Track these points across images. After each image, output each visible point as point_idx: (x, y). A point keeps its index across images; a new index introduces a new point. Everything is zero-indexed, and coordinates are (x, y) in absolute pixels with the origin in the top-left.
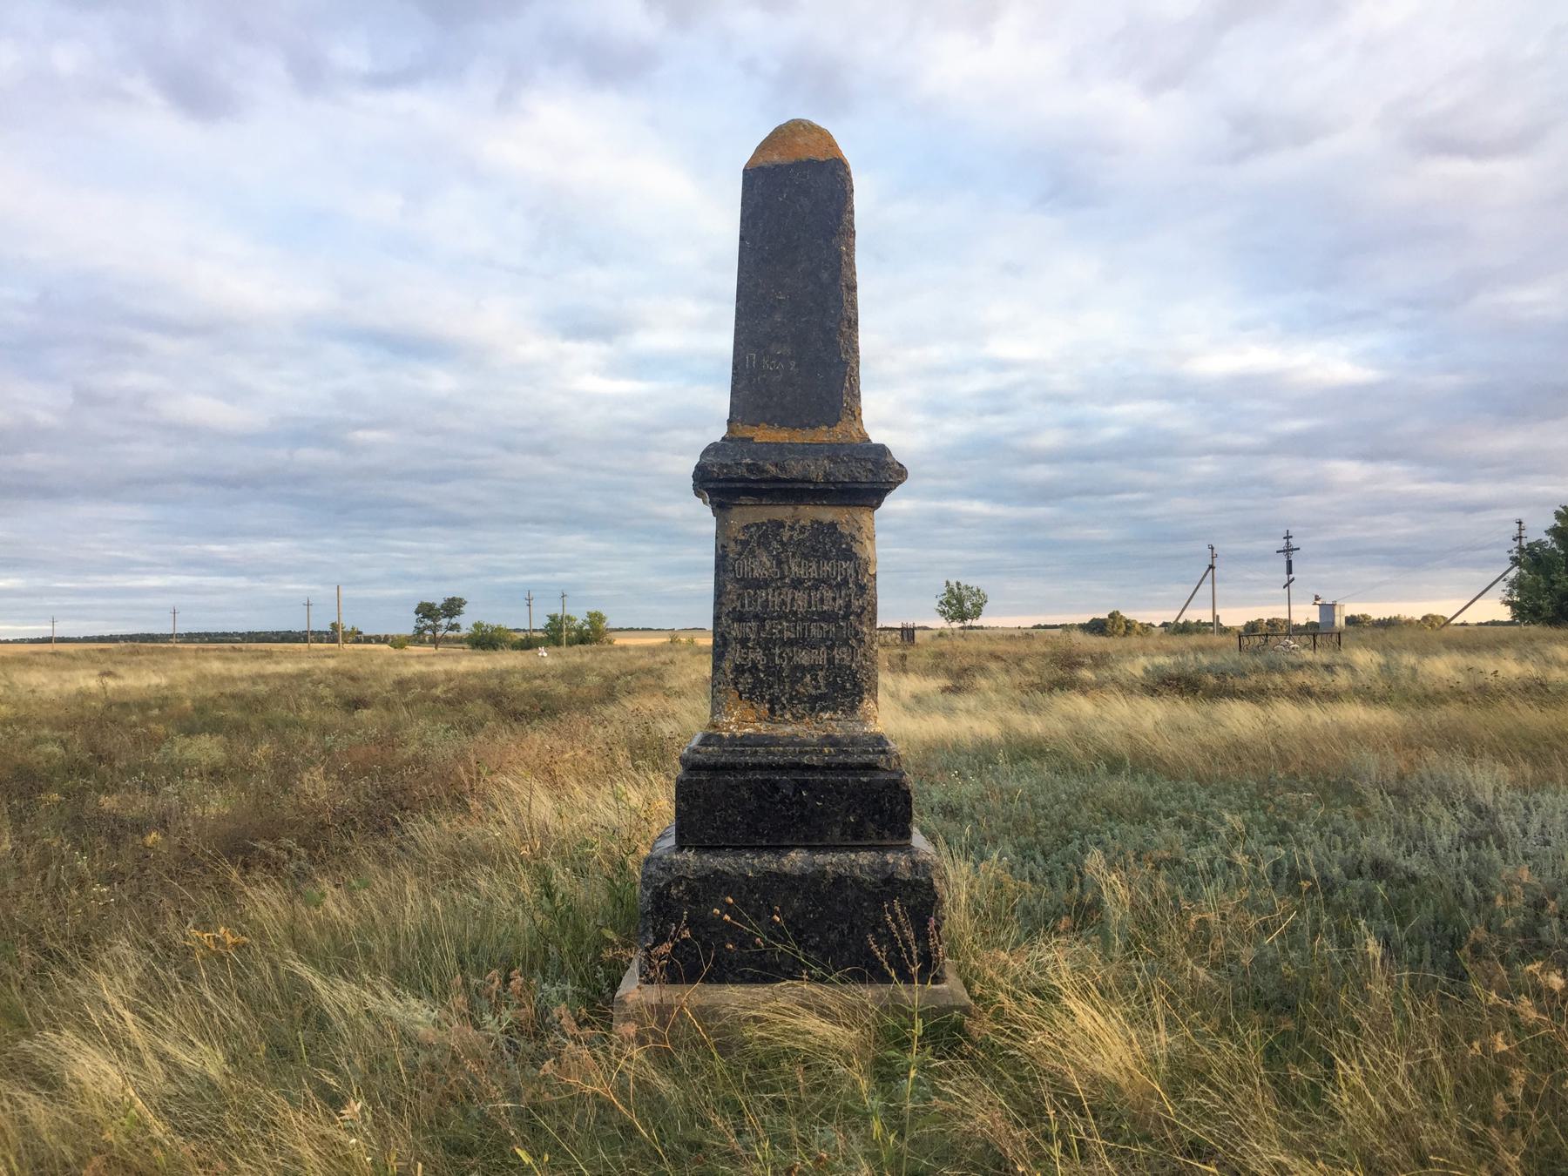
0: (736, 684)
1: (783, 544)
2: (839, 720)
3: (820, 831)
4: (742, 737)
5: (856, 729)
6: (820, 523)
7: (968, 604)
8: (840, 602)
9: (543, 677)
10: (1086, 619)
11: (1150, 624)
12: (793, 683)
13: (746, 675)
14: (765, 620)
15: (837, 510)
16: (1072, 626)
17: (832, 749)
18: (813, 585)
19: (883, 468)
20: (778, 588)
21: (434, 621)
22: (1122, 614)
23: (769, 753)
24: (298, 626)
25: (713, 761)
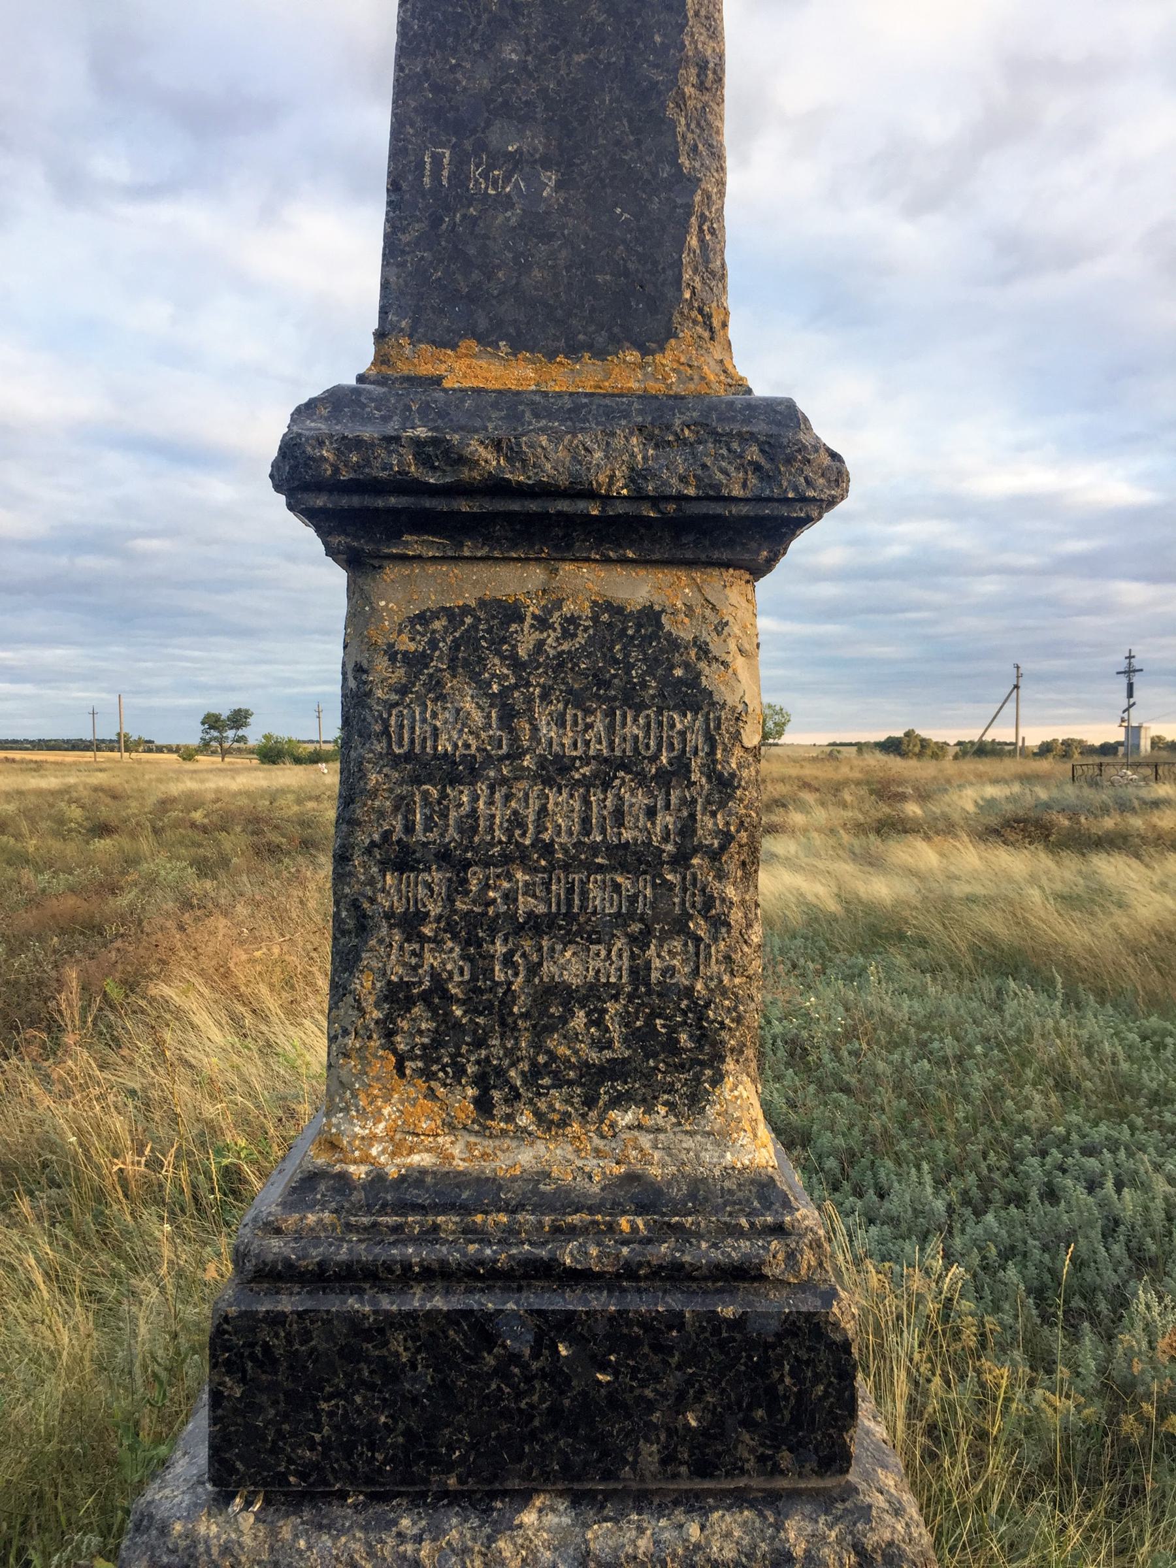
0: (389, 1034)
1: (516, 664)
2: (659, 1130)
3: (604, 1454)
4: (403, 1179)
5: (706, 1156)
6: (616, 610)
7: (770, 724)
8: (666, 819)
9: (317, 798)
10: (881, 737)
11: (945, 743)
12: (540, 1032)
13: (416, 1011)
14: (467, 865)
15: (663, 576)
16: (867, 744)
17: (640, 1221)
18: (595, 775)
19: (789, 461)
20: (504, 781)
21: (220, 732)
22: (917, 732)
23: (472, 1233)
24: (88, 736)
25: (316, 1254)
